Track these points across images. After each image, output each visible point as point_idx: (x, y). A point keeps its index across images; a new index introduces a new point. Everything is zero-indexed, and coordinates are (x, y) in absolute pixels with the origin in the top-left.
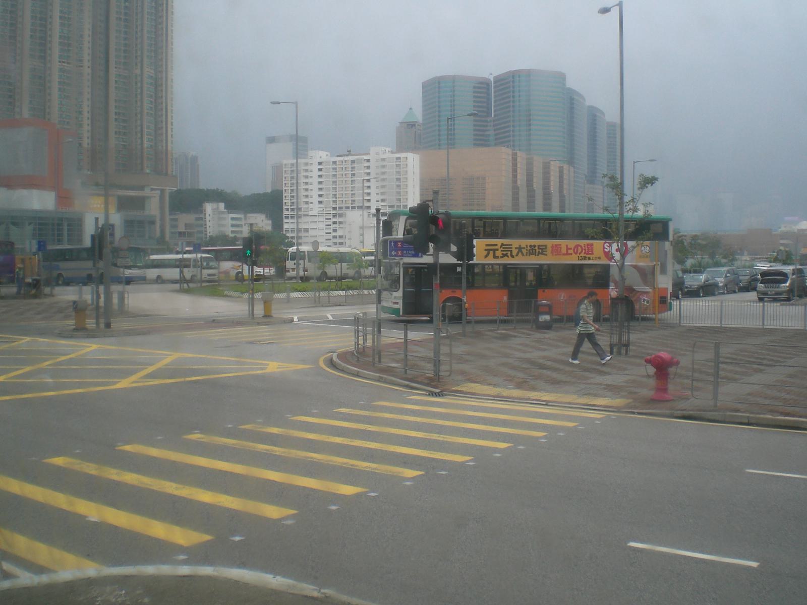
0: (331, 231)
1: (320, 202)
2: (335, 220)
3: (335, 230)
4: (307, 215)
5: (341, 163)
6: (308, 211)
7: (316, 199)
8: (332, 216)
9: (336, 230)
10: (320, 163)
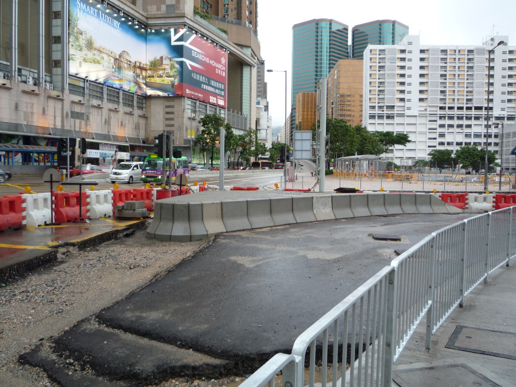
0: (436, 136)
1: (421, 100)
2: (442, 122)
3: (442, 135)
4: (402, 115)
5: (453, 53)
6: (404, 111)
7: (415, 96)
8: (438, 118)
9: (444, 135)
10: (422, 51)
